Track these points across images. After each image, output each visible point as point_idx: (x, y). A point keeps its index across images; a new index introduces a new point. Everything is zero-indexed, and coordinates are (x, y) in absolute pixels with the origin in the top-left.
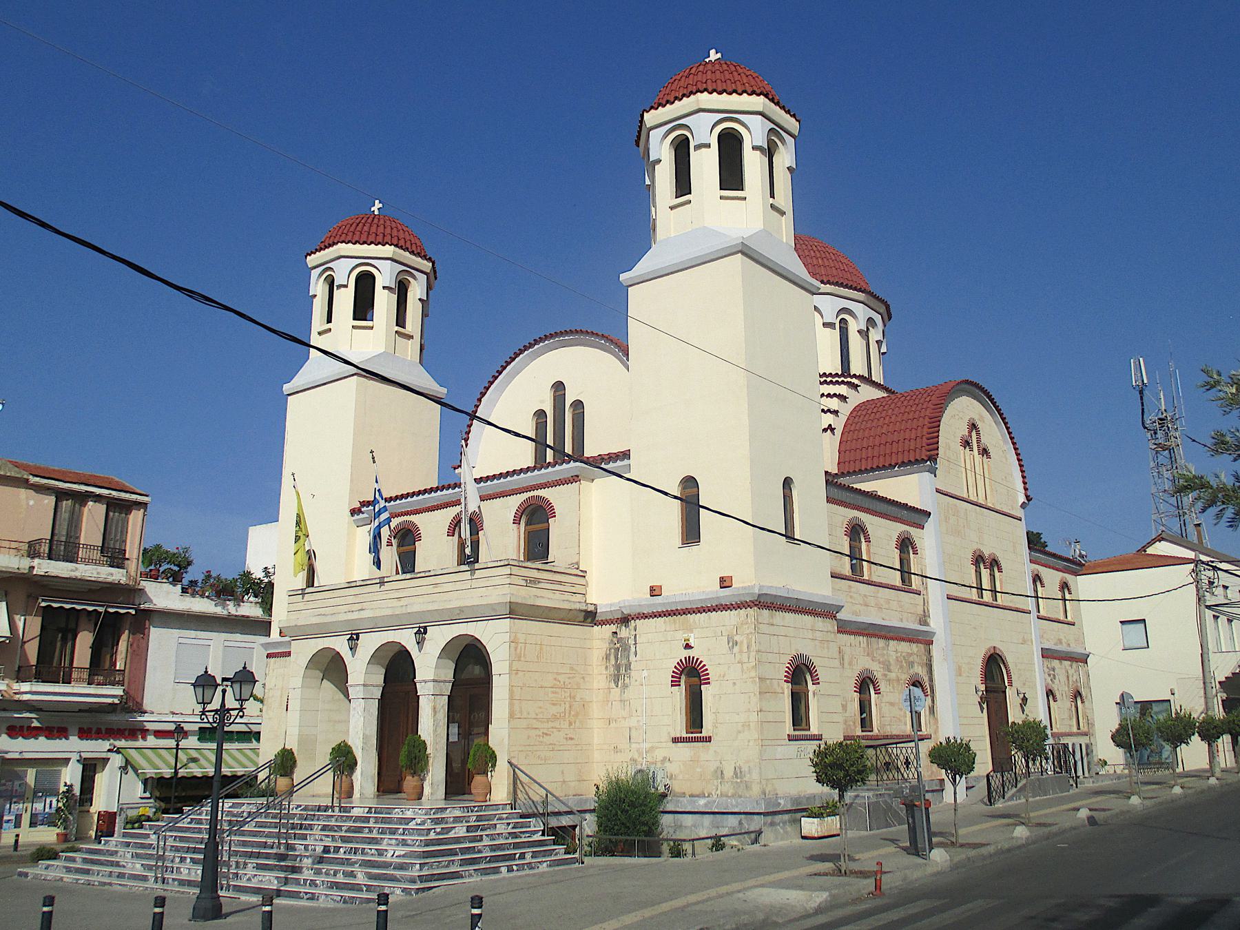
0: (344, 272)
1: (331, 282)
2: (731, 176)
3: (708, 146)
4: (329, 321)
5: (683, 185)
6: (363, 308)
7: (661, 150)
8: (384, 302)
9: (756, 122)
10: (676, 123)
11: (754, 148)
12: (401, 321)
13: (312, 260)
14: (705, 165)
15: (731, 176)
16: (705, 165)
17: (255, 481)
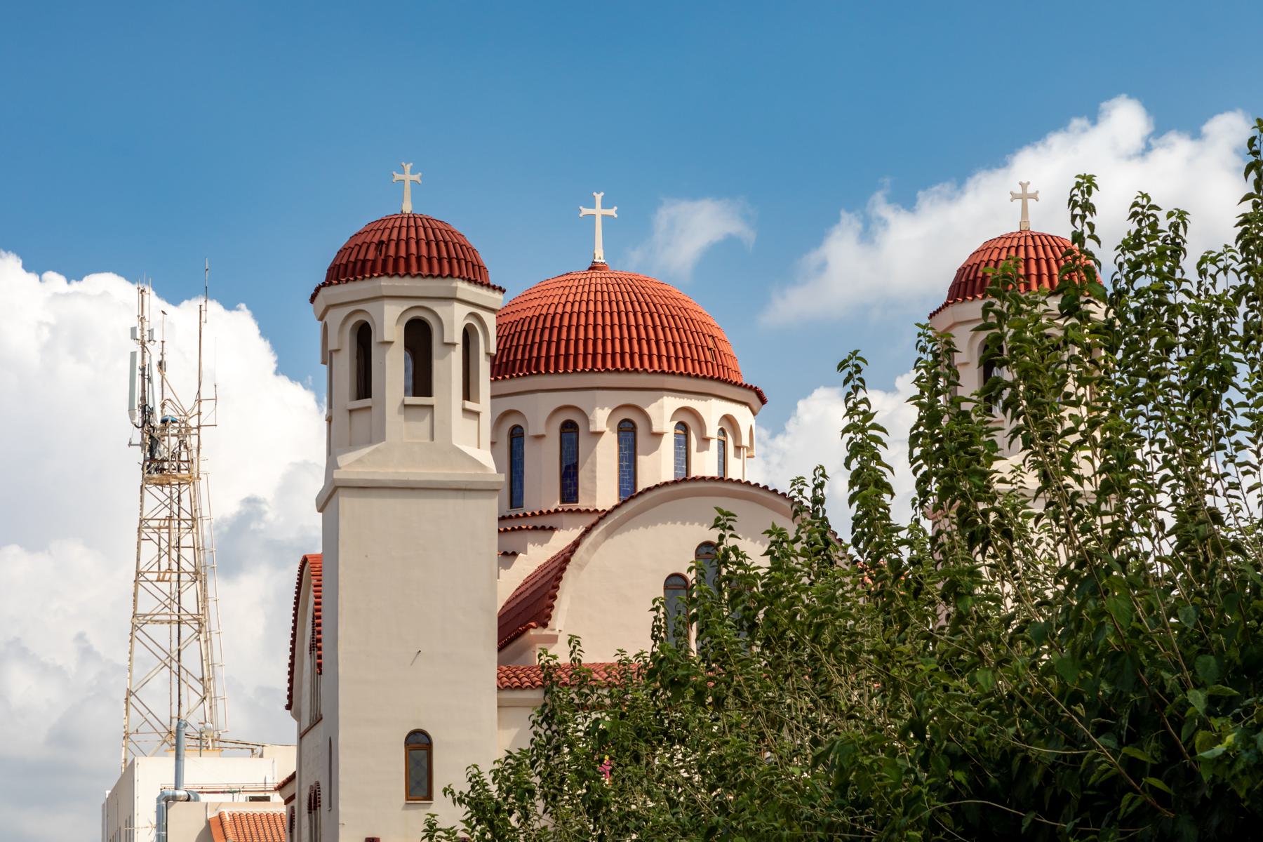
2: (421, 382)
14: (392, 366)
15: (421, 382)
16: (392, 366)
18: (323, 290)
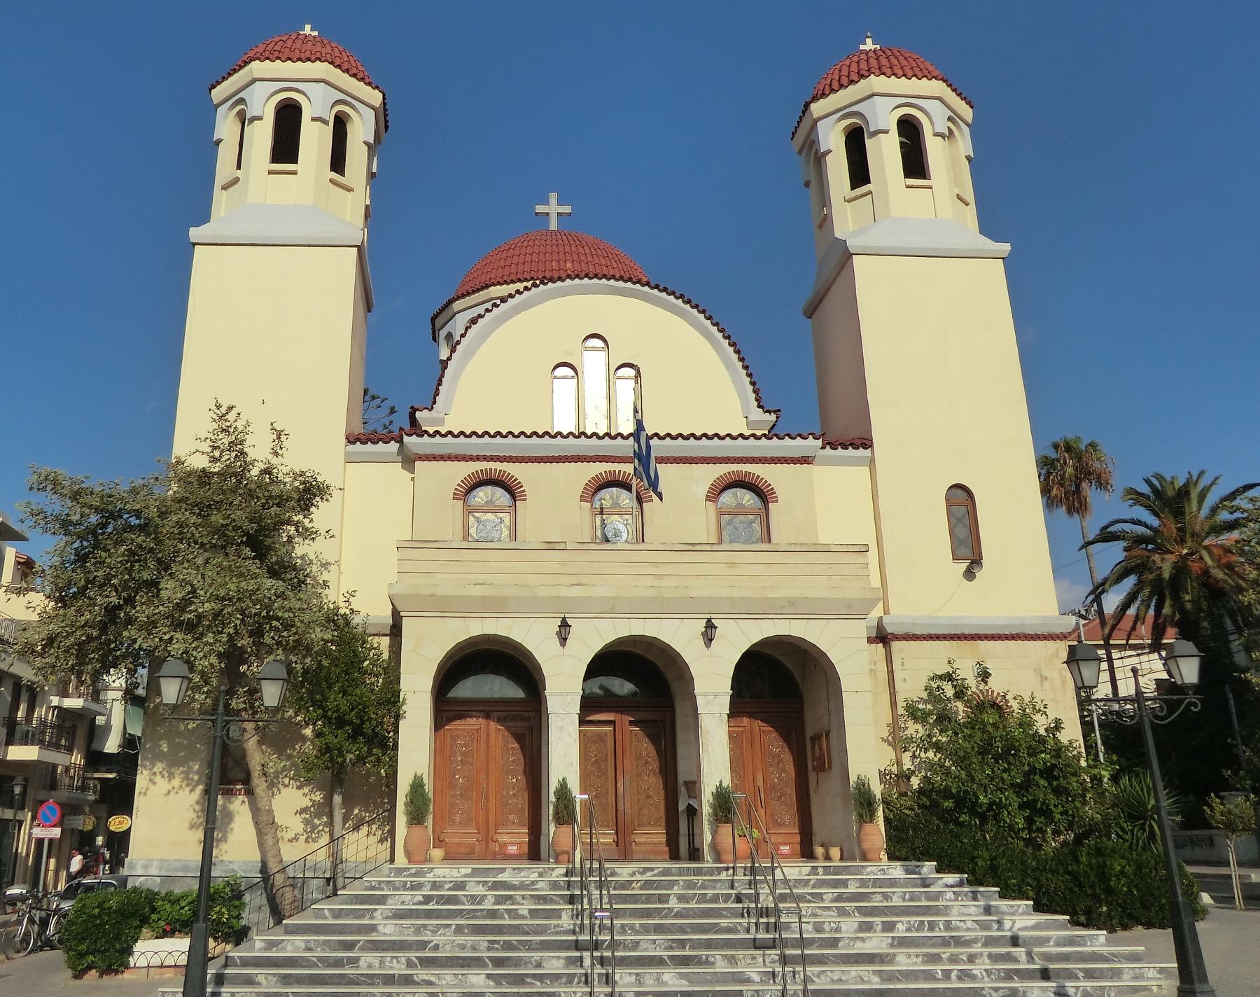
0: (263, 105)
1: (242, 118)
2: (915, 164)
3: (886, 132)
4: (239, 167)
5: (860, 174)
6: (285, 147)
7: (832, 139)
8: (314, 140)
9: (934, 107)
10: (845, 112)
11: (936, 135)
12: (338, 162)
13: (218, 94)
14: (885, 153)
15: (915, 164)
16: (885, 153)
17: (1230, 654)
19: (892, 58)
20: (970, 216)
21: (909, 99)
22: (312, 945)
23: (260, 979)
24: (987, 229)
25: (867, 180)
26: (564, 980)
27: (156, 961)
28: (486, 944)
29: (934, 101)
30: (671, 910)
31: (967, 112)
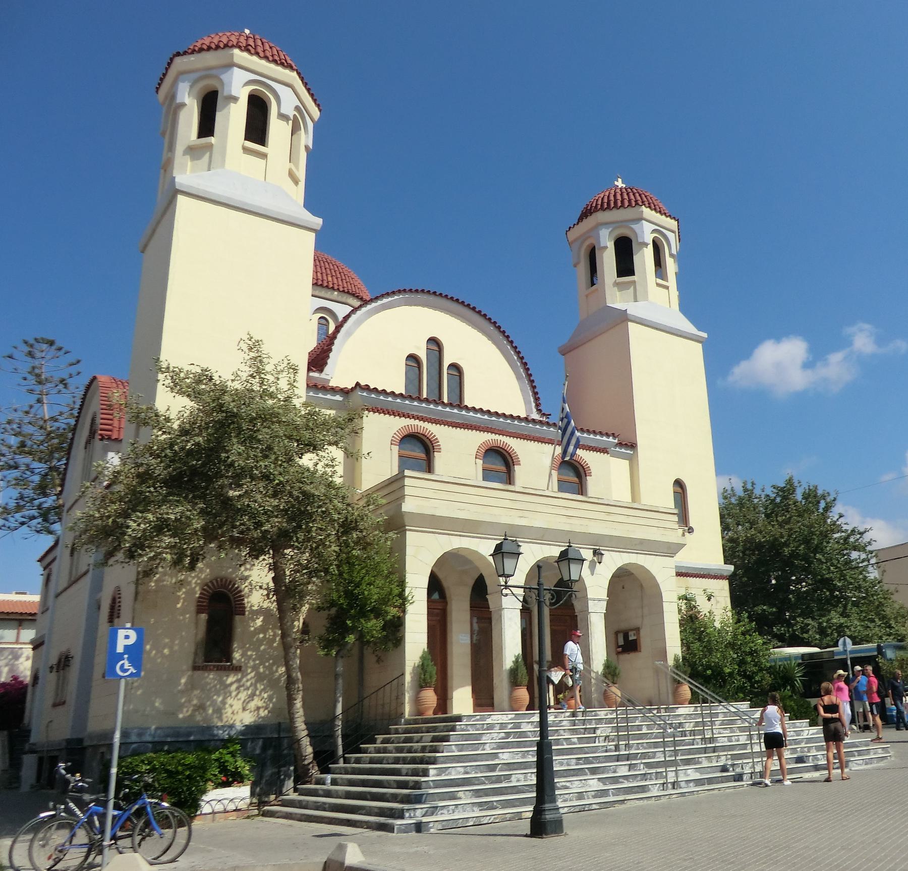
5: (207, 127)
14: (234, 118)
15: (257, 129)
16: (234, 118)
18: (178, 60)
19: (631, 194)
20: (298, 193)
21: (261, 79)
22: (468, 769)
23: (461, 794)
24: (310, 204)
25: (631, 272)
26: (639, 778)
27: (219, 807)
28: (574, 761)
29: (289, 95)
30: (340, 768)
31: (316, 113)
